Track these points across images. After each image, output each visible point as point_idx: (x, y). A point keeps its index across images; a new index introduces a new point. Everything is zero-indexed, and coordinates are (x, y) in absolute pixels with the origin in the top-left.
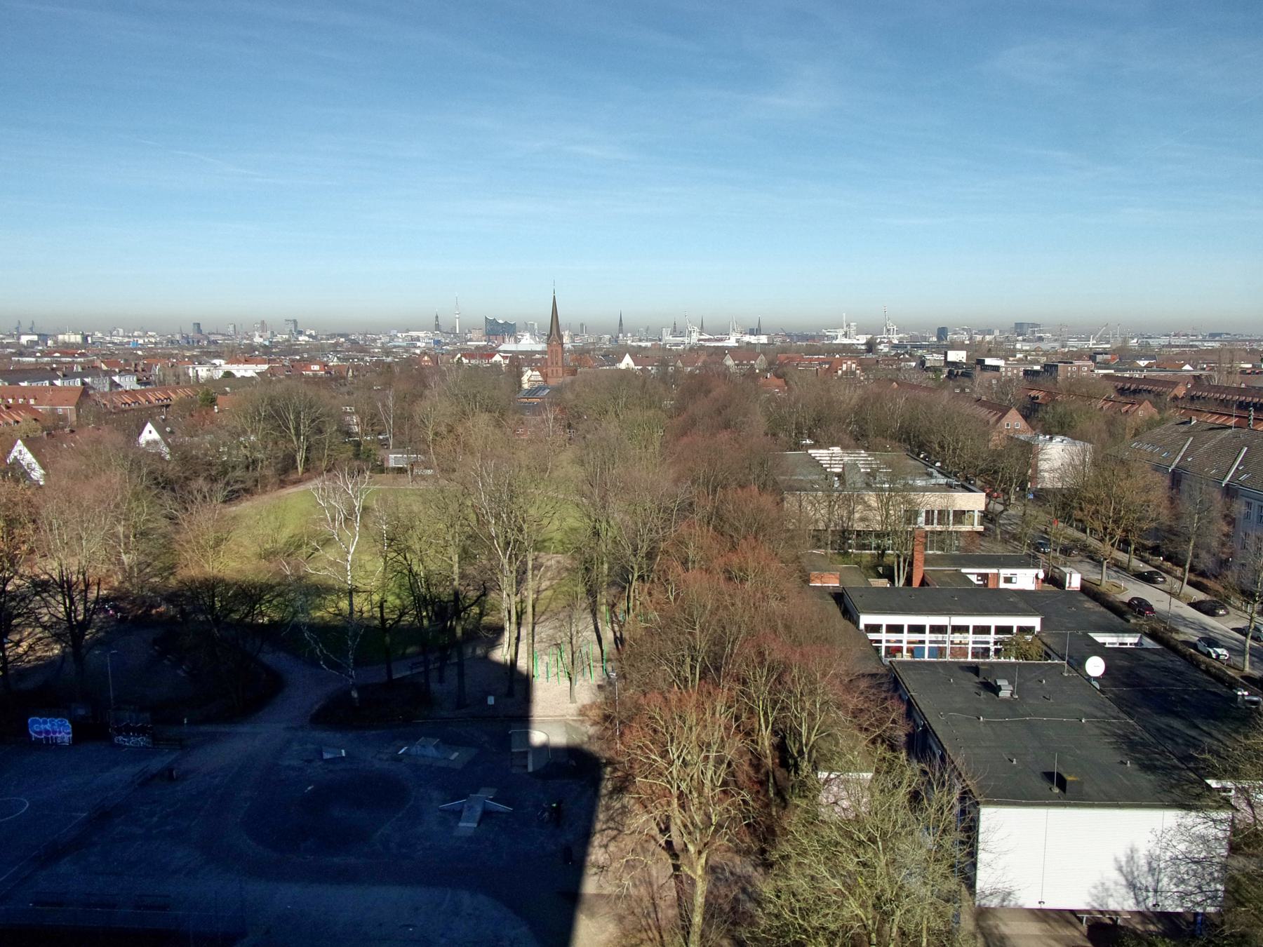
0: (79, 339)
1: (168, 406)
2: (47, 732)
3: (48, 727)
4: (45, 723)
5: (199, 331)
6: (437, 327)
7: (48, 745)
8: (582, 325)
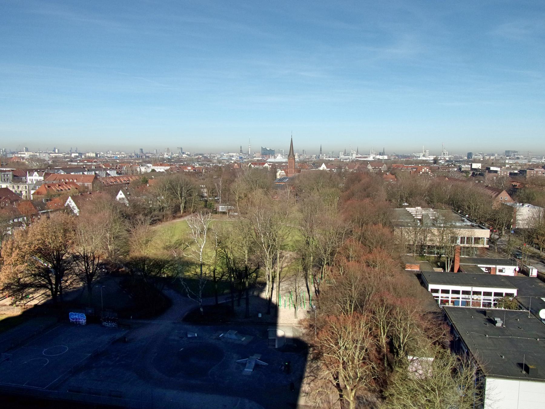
0: (94, 155)
1: (128, 183)
2: (77, 319)
3: (77, 316)
4: (76, 315)
5: (142, 152)
6: (241, 151)
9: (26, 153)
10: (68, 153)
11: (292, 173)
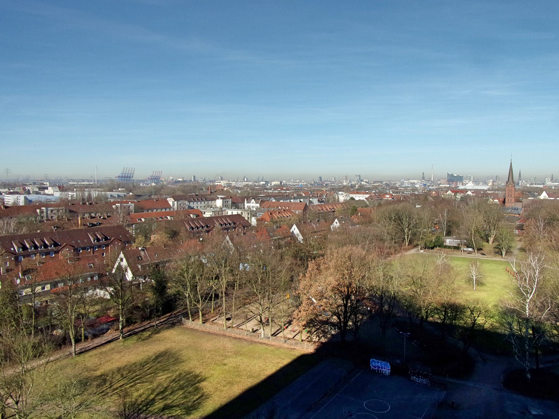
0: (279, 183)
1: (334, 212)
2: (379, 367)
3: (379, 365)
4: (378, 362)
5: (321, 180)
6: (423, 178)
7: (378, 373)
8: (497, 176)
9: (222, 182)
10: (256, 182)
11: (511, 202)
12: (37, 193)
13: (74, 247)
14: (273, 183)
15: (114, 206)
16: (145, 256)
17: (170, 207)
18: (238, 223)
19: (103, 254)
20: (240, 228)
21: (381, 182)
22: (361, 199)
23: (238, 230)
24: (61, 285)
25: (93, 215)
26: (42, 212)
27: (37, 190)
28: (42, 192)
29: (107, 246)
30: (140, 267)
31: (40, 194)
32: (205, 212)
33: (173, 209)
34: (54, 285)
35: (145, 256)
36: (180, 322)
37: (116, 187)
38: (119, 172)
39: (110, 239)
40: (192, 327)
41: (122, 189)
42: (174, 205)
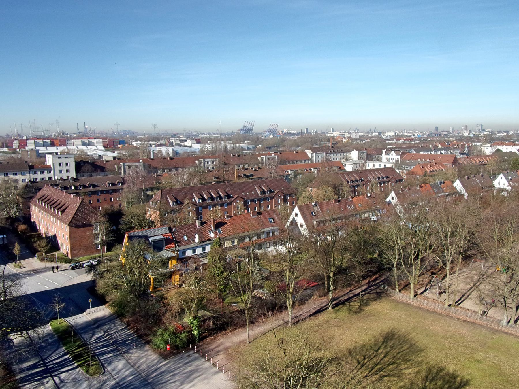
5: (437, 130)
10: (368, 133)
12: (179, 145)
13: (244, 199)
14: (387, 134)
15: (259, 158)
16: (318, 212)
17: (309, 160)
18: (391, 177)
19: (268, 207)
20: (393, 182)
21: (507, 132)
22: (513, 150)
23: (391, 184)
24: (247, 240)
25: (247, 166)
26: (200, 163)
27: (179, 142)
28: (182, 144)
29: (272, 198)
30: (315, 222)
31: (181, 146)
32: (345, 164)
33: (312, 161)
34: (242, 239)
35: (318, 212)
36: (388, 295)
37: (242, 139)
38: (240, 126)
39: (274, 192)
40: (403, 300)
41: (248, 141)
42: (312, 156)
